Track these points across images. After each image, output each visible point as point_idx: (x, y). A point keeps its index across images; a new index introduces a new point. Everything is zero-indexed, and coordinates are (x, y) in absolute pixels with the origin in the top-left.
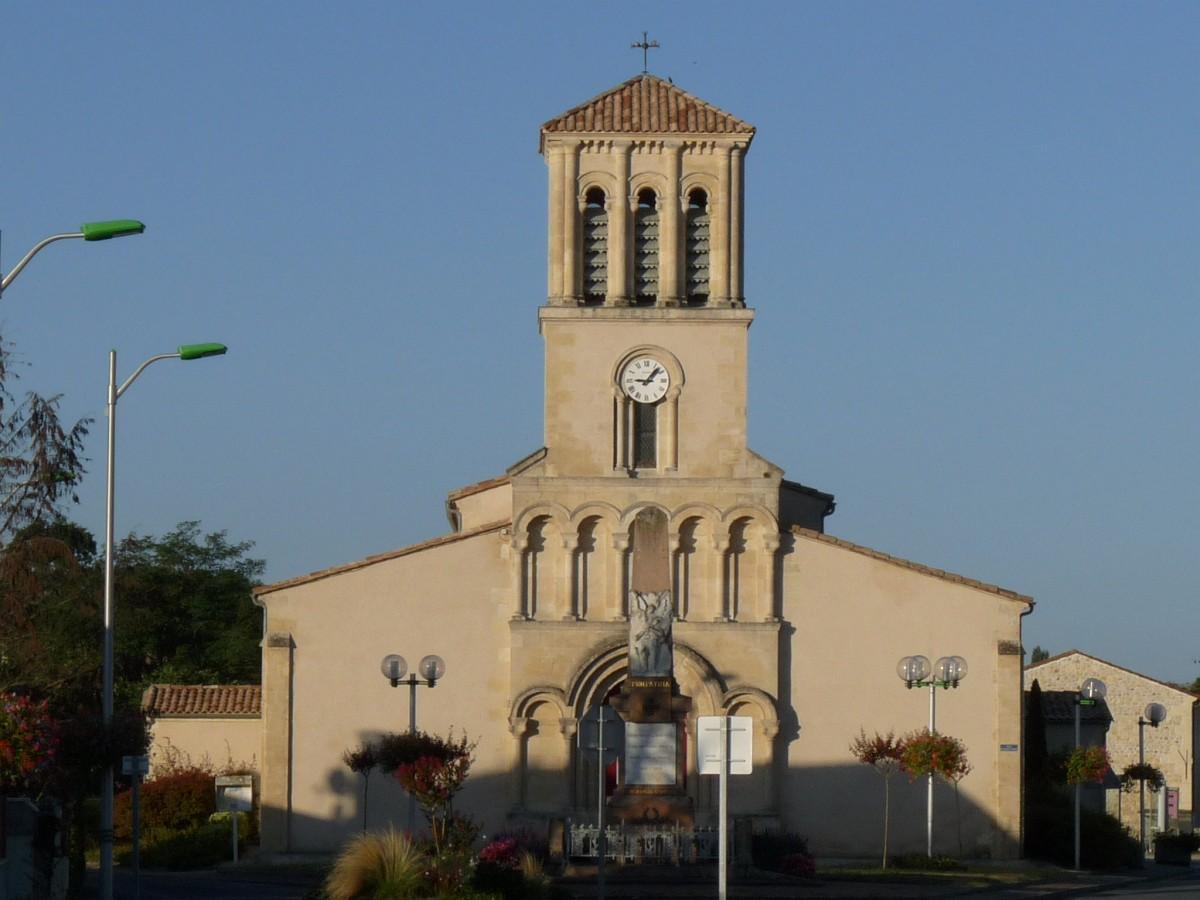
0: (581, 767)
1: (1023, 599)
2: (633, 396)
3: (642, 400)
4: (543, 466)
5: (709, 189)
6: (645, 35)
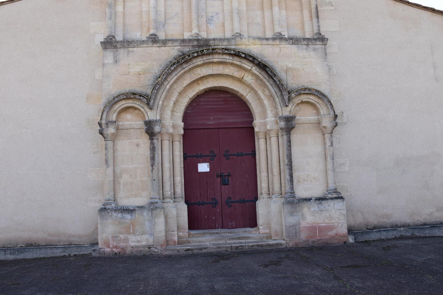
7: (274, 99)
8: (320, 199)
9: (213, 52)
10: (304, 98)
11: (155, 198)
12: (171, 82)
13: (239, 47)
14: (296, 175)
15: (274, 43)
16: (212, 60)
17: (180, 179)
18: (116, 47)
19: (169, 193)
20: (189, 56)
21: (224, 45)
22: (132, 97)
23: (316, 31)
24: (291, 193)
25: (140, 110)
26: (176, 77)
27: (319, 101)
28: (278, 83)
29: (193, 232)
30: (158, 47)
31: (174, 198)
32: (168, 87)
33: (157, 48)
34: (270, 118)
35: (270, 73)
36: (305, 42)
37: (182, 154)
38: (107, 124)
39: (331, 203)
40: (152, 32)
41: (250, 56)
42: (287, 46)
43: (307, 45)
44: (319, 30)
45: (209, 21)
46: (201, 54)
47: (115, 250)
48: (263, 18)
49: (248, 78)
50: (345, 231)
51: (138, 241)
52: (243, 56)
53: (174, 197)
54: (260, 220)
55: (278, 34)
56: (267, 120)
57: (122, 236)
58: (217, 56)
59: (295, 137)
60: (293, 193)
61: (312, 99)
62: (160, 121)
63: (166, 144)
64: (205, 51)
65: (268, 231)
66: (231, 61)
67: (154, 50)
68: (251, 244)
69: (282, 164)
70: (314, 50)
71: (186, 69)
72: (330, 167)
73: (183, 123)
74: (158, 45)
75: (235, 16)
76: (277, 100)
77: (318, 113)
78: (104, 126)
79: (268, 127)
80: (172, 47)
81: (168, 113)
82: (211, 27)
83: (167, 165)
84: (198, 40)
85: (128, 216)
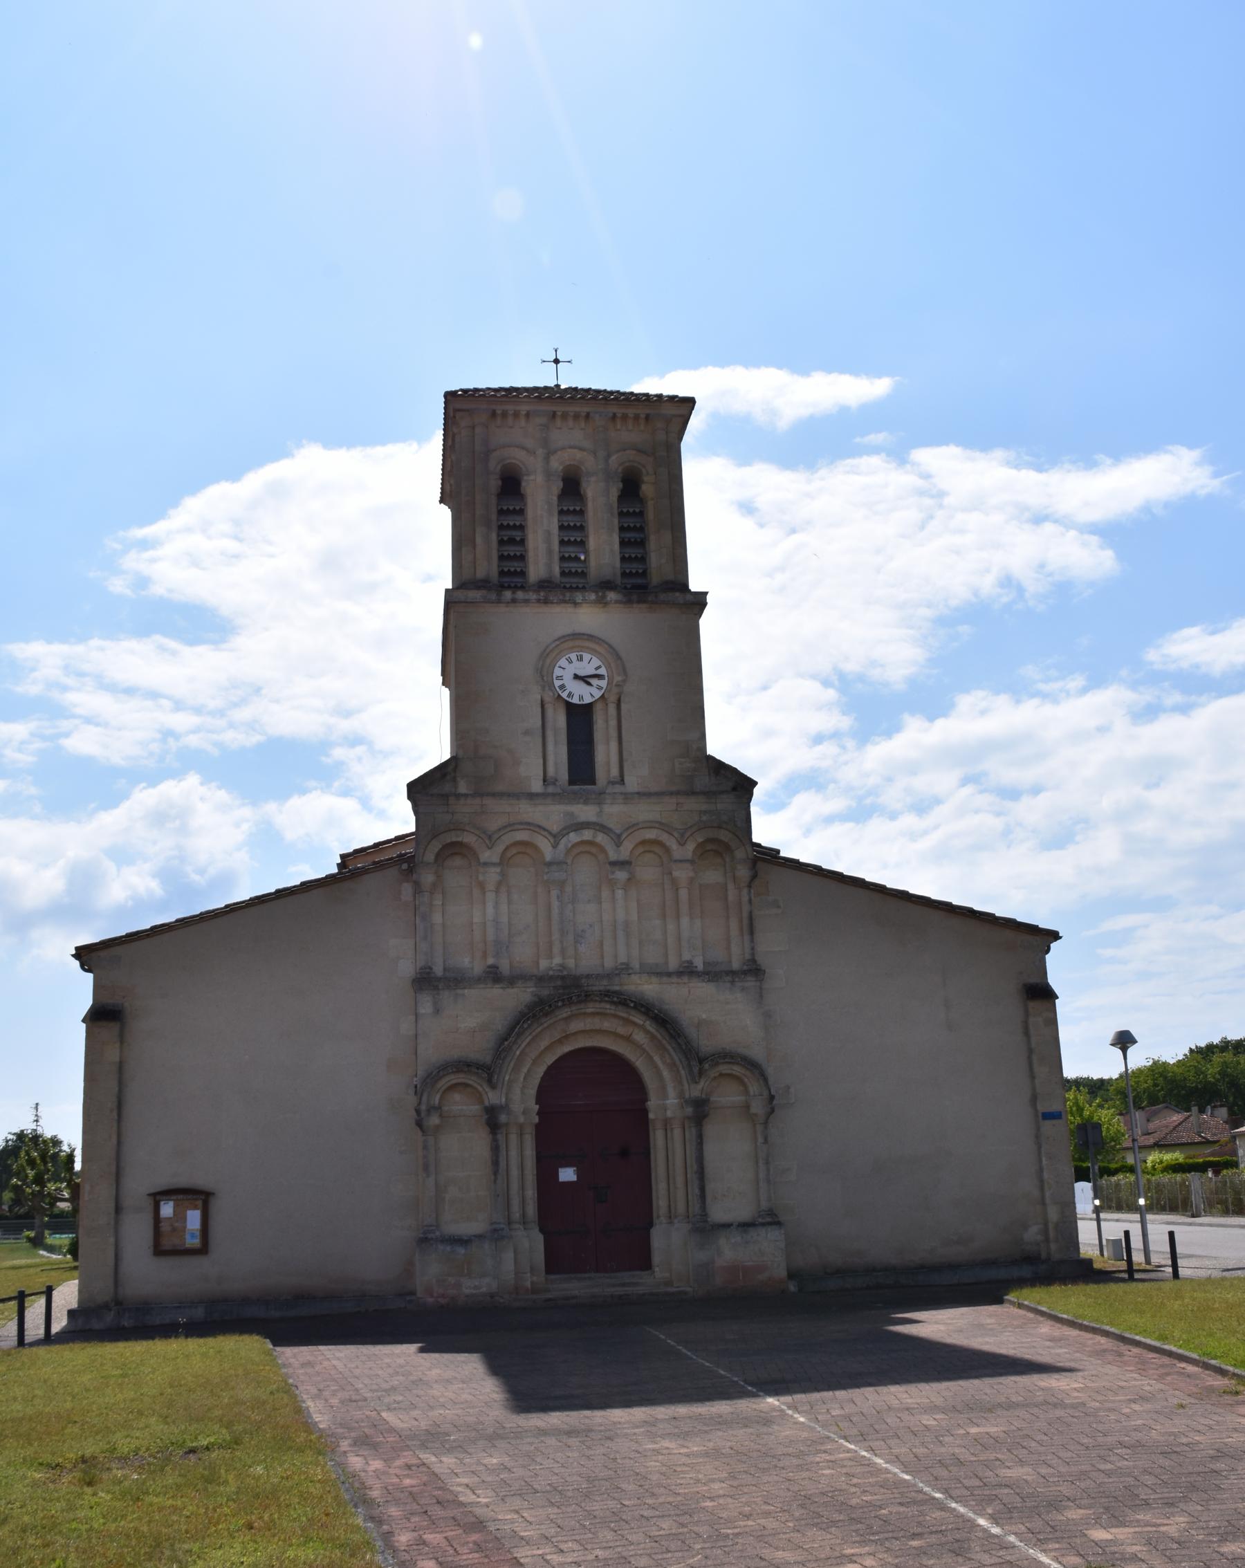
0: (1162, 1269)
1: (32, 1344)
2: (564, 695)
3: (575, 700)
4: (454, 780)
5: (644, 467)
6: (556, 351)
7: (678, 1071)
8: (745, 1226)
9: (587, 997)
10: (724, 1069)
11: (499, 1223)
12: (523, 1046)
13: (625, 987)
14: (710, 1187)
15: (680, 980)
16: (583, 1011)
17: (531, 1193)
18: (436, 988)
19: (518, 1215)
20: (550, 1006)
21: (601, 985)
22: (466, 1069)
23: (748, 957)
24: (701, 1215)
25: (475, 1088)
26: (530, 1038)
27: (748, 1073)
28: (684, 1047)
29: (553, 1277)
30: (502, 988)
31: (524, 1223)
32: (518, 1053)
33: (501, 990)
34: (672, 1101)
35: (672, 1032)
36: (729, 978)
37: (534, 1153)
38: (429, 1111)
39: (762, 1231)
40: (491, 961)
41: (642, 1006)
42: (700, 984)
43: (733, 982)
44: (753, 954)
45: (579, 938)
46: (569, 1002)
47: (442, 1301)
48: (665, 932)
49: (639, 1037)
50: (784, 1274)
51: (476, 1287)
52: (632, 1005)
53: (524, 1221)
54: (657, 1258)
55: (686, 965)
56: (668, 1102)
57: (452, 1280)
58: (591, 1005)
59: (710, 1129)
60: (704, 1214)
61: (737, 1070)
62: (507, 1105)
63: (513, 1138)
64: (574, 998)
65: (667, 1275)
66: (613, 1012)
67: (496, 992)
68: (641, 1292)
69: (689, 1171)
70: (743, 989)
71: (545, 1025)
72: (762, 1175)
73: (538, 1106)
74: (501, 985)
75: (620, 934)
76: (683, 1072)
77: (746, 1092)
78: (423, 1115)
79: (669, 1114)
80: (523, 989)
81: (516, 1094)
82: (582, 949)
83: (515, 1172)
84: (563, 978)
85: (461, 1250)
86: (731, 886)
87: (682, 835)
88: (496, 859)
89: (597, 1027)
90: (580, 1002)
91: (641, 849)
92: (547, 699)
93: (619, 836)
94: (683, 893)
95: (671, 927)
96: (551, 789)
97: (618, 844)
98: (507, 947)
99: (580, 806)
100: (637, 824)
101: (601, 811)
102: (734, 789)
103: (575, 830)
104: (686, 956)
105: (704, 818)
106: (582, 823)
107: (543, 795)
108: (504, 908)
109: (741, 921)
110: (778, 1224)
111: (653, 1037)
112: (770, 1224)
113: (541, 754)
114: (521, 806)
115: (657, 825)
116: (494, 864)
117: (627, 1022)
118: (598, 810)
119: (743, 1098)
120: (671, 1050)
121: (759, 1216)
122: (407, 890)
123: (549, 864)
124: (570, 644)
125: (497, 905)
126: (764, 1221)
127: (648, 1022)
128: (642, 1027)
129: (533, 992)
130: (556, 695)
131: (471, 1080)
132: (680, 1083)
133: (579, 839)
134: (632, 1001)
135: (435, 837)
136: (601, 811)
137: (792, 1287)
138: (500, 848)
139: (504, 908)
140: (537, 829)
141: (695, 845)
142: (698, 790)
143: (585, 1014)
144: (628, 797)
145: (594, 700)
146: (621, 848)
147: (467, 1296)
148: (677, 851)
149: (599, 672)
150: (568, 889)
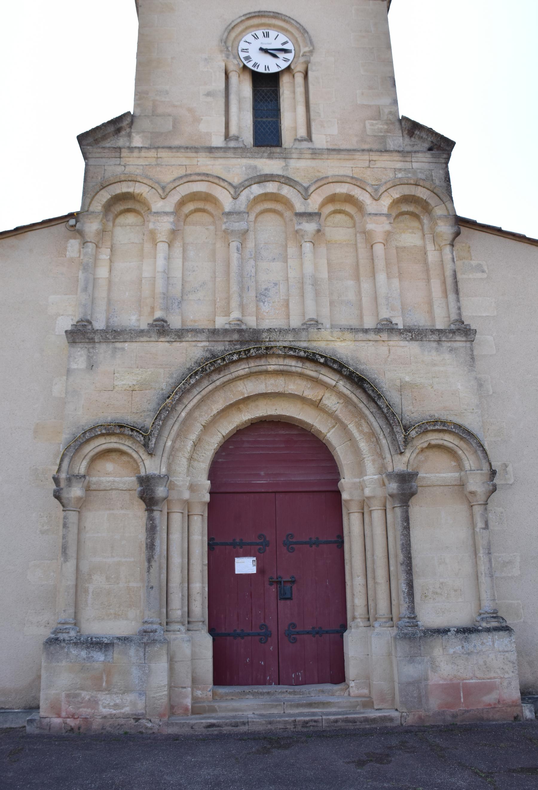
2: (250, 65)
3: (261, 70)
4: (129, 135)
7: (378, 440)
10: (434, 438)
11: (152, 623)
12: (190, 406)
13: (314, 344)
15: (377, 337)
16: (264, 368)
18: (92, 341)
19: (179, 613)
20: (223, 359)
21: (288, 340)
22: (118, 431)
23: (454, 317)
24: (409, 618)
26: (199, 397)
27: (462, 444)
28: (385, 410)
29: (222, 690)
32: (183, 414)
35: (370, 392)
36: (435, 337)
37: (206, 539)
38: (69, 480)
39: (487, 638)
40: (158, 314)
41: (335, 361)
42: (402, 343)
43: (439, 341)
44: (460, 314)
47: (71, 722)
48: (359, 293)
50: (516, 695)
51: (116, 706)
52: (322, 360)
55: (385, 323)
56: (365, 478)
57: (86, 695)
58: (273, 361)
60: (413, 618)
61: (449, 440)
62: (167, 476)
63: (177, 519)
64: (252, 351)
65: (366, 691)
66: (299, 370)
69: (392, 562)
70: (451, 350)
71: (218, 383)
72: (483, 568)
73: (209, 481)
74: (168, 339)
76: (384, 441)
77: (460, 467)
78: (63, 484)
79: (368, 492)
82: (265, 308)
83: (177, 560)
84: (240, 331)
85: (99, 656)
86: (430, 247)
87: (376, 190)
88: (170, 208)
89: (280, 389)
90: (259, 357)
91: (330, 208)
92: (231, 67)
93: (306, 189)
94: (379, 249)
95: (366, 286)
96: (232, 144)
97: (306, 198)
98: (180, 303)
99: (264, 160)
100: (327, 177)
101: (286, 166)
102: (430, 149)
103: (258, 183)
104: (385, 314)
105: (399, 175)
106: (266, 175)
107: (225, 149)
108: (178, 262)
109: (444, 282)
110: (507, 629)
111: (347, 400)
112: (497, 629)
113: (223, 113)
114: (199, 159)
115: (349, 180)
116: (166, 213)
117: (316, 381)
118: (284, 165)
119: (457, 475)
120: (370, 417)
121: (482, 619)
122: (74, 245)
123: (229, 214)
124: (256, 21)
125: (168, 258)
126: (488, 626)
127: (341, 383)
128: (332, 388)
129: (204, 346)
130: (242, 65)
131: (124, 444)
132: (381, 456)
133: (261, 191)
134: (322, 356)
135: (104, 188)
136: (286, 166)
137: (528, 713)
138: (175, 198)
139: (178, 262)
140: (216, 181)
141: (391, 201)
142: (392, 149)
143: (267, 372)
144: (316, 153)
145: (280, 69)
146: (309, 201)
147: (105, 717)
148: (370, 205)
149: (285, 47)
150: (250, 245)
